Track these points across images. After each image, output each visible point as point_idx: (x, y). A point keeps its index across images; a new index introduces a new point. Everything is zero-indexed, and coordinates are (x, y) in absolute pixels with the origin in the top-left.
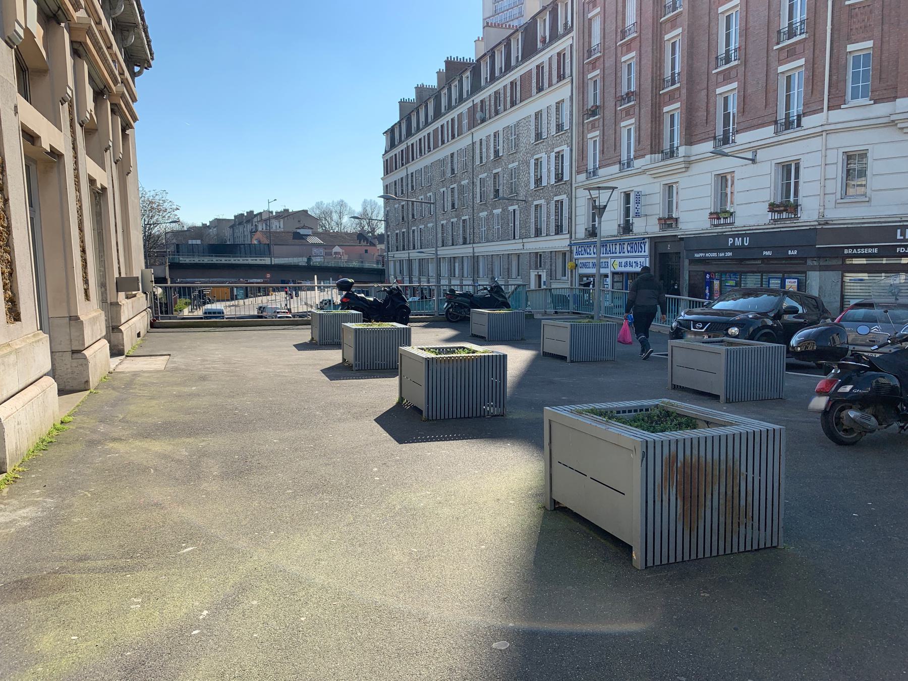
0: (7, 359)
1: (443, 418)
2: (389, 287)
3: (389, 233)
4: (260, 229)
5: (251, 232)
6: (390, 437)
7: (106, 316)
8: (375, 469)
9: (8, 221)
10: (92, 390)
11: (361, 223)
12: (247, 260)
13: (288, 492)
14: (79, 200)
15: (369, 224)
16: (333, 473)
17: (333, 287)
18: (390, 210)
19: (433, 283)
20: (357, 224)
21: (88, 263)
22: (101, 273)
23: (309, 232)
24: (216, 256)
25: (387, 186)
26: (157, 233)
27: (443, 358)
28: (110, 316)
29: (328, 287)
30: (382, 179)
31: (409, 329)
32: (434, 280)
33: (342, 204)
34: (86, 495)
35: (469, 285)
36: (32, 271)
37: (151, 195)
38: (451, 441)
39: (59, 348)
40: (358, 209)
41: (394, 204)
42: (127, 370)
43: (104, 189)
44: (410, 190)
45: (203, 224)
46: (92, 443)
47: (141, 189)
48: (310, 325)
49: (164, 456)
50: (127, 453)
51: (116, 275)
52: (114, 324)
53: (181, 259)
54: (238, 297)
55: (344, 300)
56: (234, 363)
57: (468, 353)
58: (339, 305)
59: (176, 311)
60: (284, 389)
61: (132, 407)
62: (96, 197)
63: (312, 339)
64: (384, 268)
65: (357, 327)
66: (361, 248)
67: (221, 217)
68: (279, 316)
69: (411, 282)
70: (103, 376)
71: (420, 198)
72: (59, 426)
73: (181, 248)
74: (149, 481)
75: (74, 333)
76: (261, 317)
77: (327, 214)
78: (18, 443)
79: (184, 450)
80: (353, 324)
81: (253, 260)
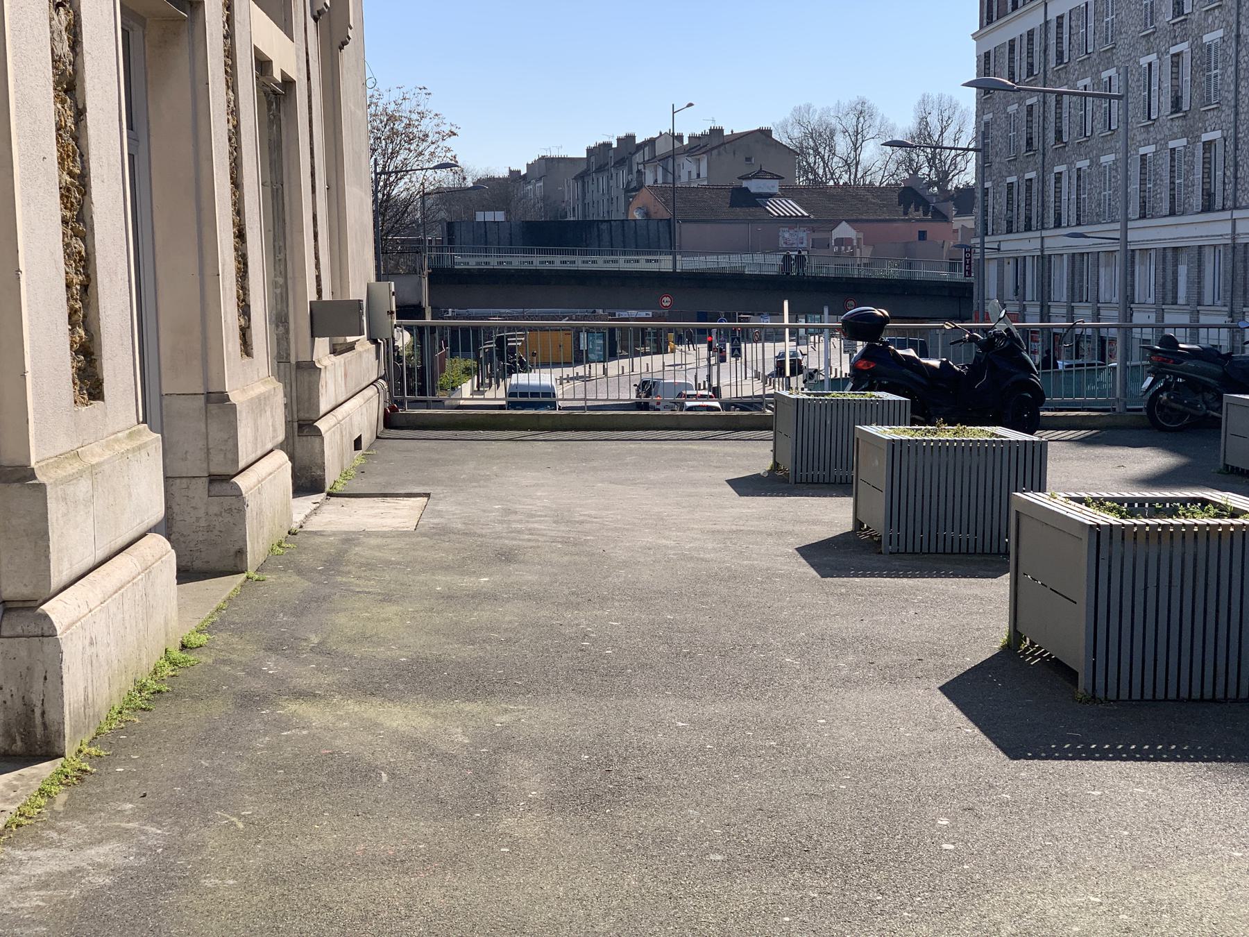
0: (72, 488)
1: (1136, 695)
2: (985, 331)
3: (988, 185)
4: (649, 180)
5: (628, 190)
6: (982, 737)
7: (285, 396)
8: (944, 822)
9: (82, 162)
10: (251, 572)
11: (911, 160)
12: (616, 262)
13: (712, 857)
14: (234, 111)
15: (931, 161)
16: (829, 820)
17: (832, 332)
18: (994, 120)
19: (1111, 318)
20: (899, 163)
21: (249, 264)
22: (278, 291)
23: (772, 186)
24: (540, 252)
25: (987, 55)
26: (404, 195)
27: (1142, 527)
28: (294, 394)
29: (820, 331)
30: (976, 37)
31: (1042, 446)
32: (1116, 313)
33: (861, 111)
34: (232, 823)
35: (1219, 327)
36: (130, 281)
37: (392, 99)
38: (1160, 764)
39: (181, 468)
40: (904, 125)
41: (1008, 104)
42: (330, 528)
43: (288, 83)
44: (1052, 64)
45: (510, 171)
46: (248, 701)
47: (370, 84)
48: (770, 429)
49: (413, 743)
50: (327, 729)
51: (312, 296)
52: (304, 415)
53: (458, 259)
54: (591, 356)
55: (862, 365)
56: (582, 522)
57: (1218, 516)
58: (845, 380)
59: (442, 388)
60: (704, 594)
61: (341, 619)
62: (270, 104)
63: (776, 465)
64: (972, 279)
65: (897, 437)
66: (906, 230)
67: (555, 153)
68: (689, 404)
69: (1045, 316)
70: (276, 542)
71: (1080, 84)
72: (176, 654)
73: (457, 233)
74: (376, 801)
75: (216, 433)
76: (646, 406)
77: (821, 138)
78: (90, 689)
79: (459, 730)
80: (886, 428)
81: (629, 261)
